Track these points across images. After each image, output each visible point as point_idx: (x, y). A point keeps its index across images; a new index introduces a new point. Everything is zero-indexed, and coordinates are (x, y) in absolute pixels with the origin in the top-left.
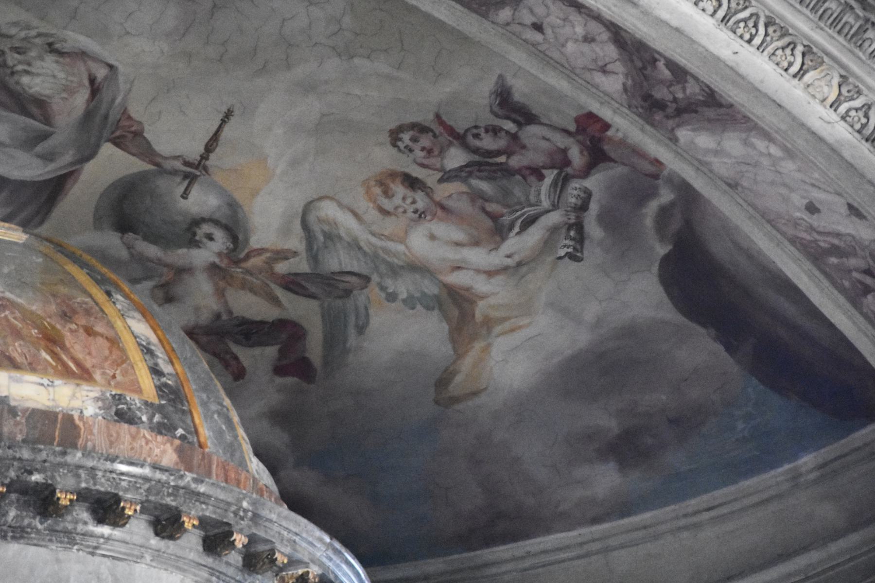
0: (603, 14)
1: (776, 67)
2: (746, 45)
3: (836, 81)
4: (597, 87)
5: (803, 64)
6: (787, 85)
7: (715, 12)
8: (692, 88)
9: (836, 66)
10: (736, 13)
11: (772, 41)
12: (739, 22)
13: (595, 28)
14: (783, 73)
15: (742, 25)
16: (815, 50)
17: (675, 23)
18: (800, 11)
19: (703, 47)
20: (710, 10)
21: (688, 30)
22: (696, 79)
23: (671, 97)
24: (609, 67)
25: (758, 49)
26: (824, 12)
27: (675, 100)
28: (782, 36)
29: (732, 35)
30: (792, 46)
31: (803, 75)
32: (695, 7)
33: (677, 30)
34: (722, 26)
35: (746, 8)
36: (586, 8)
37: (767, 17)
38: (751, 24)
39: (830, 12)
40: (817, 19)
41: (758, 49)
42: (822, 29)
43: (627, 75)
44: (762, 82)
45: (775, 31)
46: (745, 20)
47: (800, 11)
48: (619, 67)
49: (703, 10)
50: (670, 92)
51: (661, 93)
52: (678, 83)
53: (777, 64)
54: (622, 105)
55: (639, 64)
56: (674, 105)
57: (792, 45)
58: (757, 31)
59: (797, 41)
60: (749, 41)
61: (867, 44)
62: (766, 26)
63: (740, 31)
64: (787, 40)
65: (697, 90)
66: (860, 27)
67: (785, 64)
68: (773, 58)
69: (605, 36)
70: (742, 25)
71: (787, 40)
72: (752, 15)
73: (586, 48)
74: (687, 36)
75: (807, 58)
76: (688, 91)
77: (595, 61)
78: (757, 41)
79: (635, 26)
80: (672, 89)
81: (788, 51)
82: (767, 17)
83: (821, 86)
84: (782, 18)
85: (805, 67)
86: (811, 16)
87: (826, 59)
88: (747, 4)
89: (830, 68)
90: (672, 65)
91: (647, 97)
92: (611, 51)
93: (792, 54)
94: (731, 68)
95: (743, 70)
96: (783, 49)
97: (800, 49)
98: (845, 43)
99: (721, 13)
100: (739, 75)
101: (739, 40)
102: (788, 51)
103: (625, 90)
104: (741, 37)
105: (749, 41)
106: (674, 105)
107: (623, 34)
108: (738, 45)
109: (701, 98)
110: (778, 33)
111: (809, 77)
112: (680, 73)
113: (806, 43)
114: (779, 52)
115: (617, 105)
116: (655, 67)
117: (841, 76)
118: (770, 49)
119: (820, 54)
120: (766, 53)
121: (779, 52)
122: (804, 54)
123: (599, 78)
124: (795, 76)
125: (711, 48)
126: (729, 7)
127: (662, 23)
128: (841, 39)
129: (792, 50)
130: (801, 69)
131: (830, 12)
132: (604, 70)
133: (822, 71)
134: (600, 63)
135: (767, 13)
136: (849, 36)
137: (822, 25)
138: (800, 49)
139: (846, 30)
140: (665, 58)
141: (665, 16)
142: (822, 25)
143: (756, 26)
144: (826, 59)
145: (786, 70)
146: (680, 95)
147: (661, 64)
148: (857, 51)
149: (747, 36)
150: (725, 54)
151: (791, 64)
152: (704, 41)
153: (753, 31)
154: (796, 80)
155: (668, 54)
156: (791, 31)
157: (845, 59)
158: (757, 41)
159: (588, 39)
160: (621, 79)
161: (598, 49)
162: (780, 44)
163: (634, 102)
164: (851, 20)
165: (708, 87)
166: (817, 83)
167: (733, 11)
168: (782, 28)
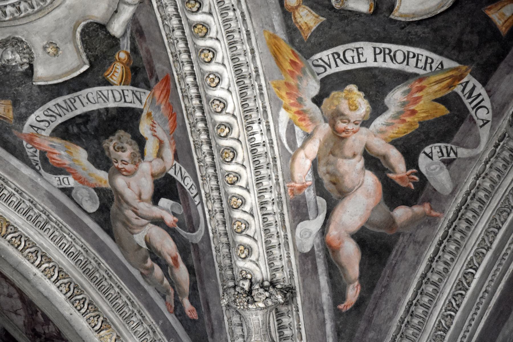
0: (16, 284)
1: (88, 325)
2: (77, 312)
3: (114, 337)
4: (12, 321)
5: (101, 326)
6: (90, 332)
7: (66, 293)
8: (52, 328)
9: (116, 331)
10: (76, 295)
11: (90, 312)
12: (76, 300)
13: (13, 291)
14: (91, 329)
15: (77, 302)
16: (108, 321)
17: (46, 294)
18: (104, 301)
19: (57, 308)
20: (65, 291)
21: (51, 298)
22: (54, 325)
23: (43, 332)
24: (18, 312)
25: (82, 315)
26: (116, 303)
27: (45, 333)
28: (95, 311)
29: (72, 306)
30: (98, 316)
31: (100, 331)
32: (57, 289)
33: (46, 297)
34: (68, 300)
35: (81, 294)
36: (9, 280)
37: (90, 301)
38: (82, 302)
39: (118, 305)
40: (111, 307)
41: (82, 315)
42: (113, 312)
43: (25, 317)
44: (80, 330)
45: (92, 308)
46: (79, 300)
47: (104, 301)
48: (22, 312)
49: (61, 291)
50: (43, 329)
51: (39, 329)
52: (46, 325)
53: (90, 324)
54: (23, 332)
55: (30, 312)
56: (44, 336)
57: (99, 316)
58: (84, 306)
59: (101, 315)
60: (79, 310)
61: (131, 323)
62: (88, 305)
63: (76, 305)
64: (97, 313)
65: (54, 330)
66: (130, 314)
67: (93, 325)
68: (88, 320)
69: (16, 295)
70: (77, 302)
71: (97, 313)
72: (83, 298)
73: (8, 299)
74: (50, 301)
75: (90, 307)
76: (50, 330)
77: (12, 307)
78: (83, 311)
79: (29, 292)
80: (44, 327)
81: (96, 319)
82: (90, 301)
83: (107, 339)
84: (97, 303)
85: (102, 328)
86: (110, 305)
87: (112, 326)
88: (82, 292)
89: (113, 331)
90: (44, 315)
91: (34, 330)
92: (18, 304)
93: (97, 321)
94: (67, 321)
95: (72, 323)
96: (65, 284)
97: (101, 318)
98: (122, 320)
99: (69, 294)
100: (71, 325)
101: (74, 309)
102: (96, 319)
103: (25, 325)
104: (76, 307)
105: (79, 310)
106: (44, 336)
107: (24, 295)
108: (73, 310)
109: (55, 334)
110: (93, 309)
111: (103, 333)
112: (47, 320)
113: (105, 317)
114: (92, 318)
115: (21, 332)
116: (37, 315)
117: (117, 336)
118: (58, 284)
119: (110, 323)
120: (85, 317)
121: (92, 318)
122: (102, 322)
123: (13, 316)
124: (96, 331)
125: (60, 309)
126: (73, 292)
127: (39, 292)
128: (120, 318)
129: (98, 318)
130: (100, 328)
131: (118, 305)
132: (16, 313)
133: (109, 332)
134: (15, 309)
135: (91, 299)
136: (124, 318)
137: (114, 310)
138: (101, 318)
139: (123, 315)
140: (42, 311)
141: (42, 289)
142: (114, 310)
143: (84, 304)
144: (112, 326)
145: (93, 327)
146: (47, 331)
147: (39, 314)
148: (126, 325)
149: (79, 308)
150: (66, 313)
151: (95, 325)
152: (57, 305)
153: (82, 306)
154: (96, 333)
155: (43, 309)
156: (99, 310)
157: (121, 328)
158: (83, 311)
159: (10, 296)
160: (23, 318)
161: (13, 302)
162: (93, 314)
163: (28, 332)
164: (127, 310)
165: (58, 329)
166: (105, 337)
167: (75, 294)
168: (95, 307)
